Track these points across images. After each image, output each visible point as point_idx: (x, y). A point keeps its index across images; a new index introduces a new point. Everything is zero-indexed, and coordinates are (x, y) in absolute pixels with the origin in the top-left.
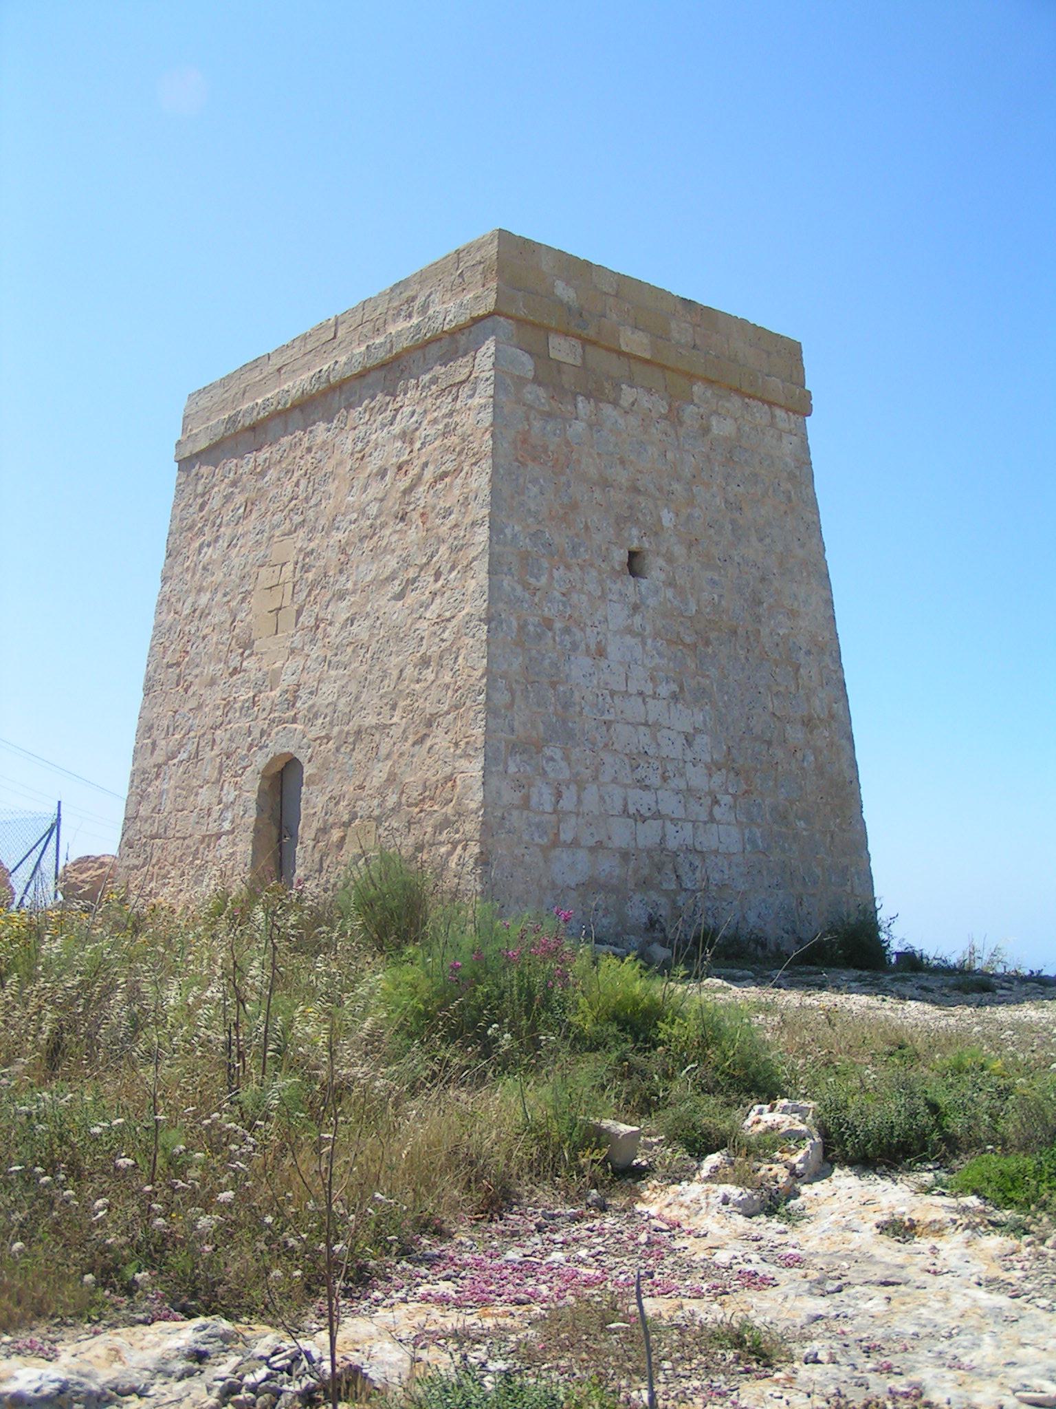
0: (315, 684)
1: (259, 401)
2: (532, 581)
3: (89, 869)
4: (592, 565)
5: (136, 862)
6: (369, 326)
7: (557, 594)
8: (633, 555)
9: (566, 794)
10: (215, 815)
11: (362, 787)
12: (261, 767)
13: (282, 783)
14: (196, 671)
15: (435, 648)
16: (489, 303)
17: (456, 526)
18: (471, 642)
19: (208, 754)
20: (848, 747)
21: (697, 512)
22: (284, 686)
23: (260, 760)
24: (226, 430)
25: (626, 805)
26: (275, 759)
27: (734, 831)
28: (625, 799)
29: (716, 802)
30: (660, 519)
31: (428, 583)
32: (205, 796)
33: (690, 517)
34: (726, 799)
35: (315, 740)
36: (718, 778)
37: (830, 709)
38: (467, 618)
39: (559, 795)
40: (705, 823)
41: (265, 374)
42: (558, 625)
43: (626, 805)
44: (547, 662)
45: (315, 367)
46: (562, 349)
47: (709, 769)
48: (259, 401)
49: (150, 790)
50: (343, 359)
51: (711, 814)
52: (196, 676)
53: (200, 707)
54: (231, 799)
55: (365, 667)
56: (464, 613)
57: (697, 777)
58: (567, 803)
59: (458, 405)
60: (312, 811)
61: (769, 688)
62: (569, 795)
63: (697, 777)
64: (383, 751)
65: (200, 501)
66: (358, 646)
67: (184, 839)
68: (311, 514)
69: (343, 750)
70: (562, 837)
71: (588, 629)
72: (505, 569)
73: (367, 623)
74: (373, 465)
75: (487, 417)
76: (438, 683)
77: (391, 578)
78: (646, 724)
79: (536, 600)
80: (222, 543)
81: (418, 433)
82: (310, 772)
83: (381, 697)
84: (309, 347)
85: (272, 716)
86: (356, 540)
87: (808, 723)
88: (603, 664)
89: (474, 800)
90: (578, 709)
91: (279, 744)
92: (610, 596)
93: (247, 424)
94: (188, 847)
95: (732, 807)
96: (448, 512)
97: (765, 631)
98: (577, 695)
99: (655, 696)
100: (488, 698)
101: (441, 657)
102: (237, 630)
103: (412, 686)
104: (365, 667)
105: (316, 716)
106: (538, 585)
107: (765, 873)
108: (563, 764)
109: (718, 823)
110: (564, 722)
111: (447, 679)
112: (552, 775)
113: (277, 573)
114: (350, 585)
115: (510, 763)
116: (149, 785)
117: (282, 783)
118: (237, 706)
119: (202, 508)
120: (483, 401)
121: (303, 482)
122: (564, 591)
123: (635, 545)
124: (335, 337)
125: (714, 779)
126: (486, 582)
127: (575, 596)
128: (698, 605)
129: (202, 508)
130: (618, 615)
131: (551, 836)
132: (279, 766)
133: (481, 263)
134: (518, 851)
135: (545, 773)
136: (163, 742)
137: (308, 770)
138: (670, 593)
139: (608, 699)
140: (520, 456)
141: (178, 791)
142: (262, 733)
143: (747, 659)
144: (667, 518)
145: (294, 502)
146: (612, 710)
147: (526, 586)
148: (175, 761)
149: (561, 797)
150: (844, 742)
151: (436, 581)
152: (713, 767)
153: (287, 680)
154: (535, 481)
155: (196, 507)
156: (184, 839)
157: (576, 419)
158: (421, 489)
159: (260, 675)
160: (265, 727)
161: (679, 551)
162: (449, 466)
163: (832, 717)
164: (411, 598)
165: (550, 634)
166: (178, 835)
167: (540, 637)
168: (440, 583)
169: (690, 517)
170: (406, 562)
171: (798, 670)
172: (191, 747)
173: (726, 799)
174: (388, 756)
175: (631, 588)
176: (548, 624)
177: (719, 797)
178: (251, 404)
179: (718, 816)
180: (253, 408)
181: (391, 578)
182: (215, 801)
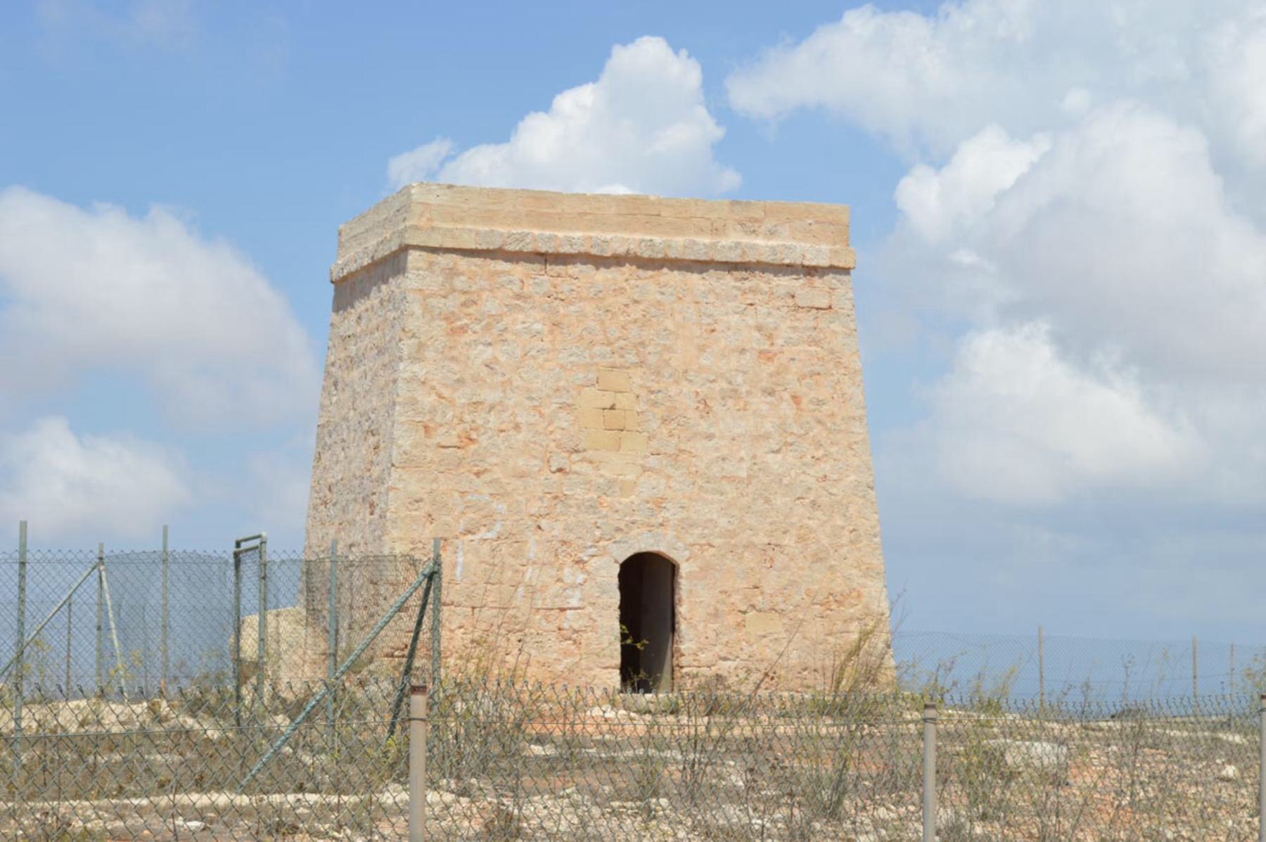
83: (771, 524)
137: (684, 569)
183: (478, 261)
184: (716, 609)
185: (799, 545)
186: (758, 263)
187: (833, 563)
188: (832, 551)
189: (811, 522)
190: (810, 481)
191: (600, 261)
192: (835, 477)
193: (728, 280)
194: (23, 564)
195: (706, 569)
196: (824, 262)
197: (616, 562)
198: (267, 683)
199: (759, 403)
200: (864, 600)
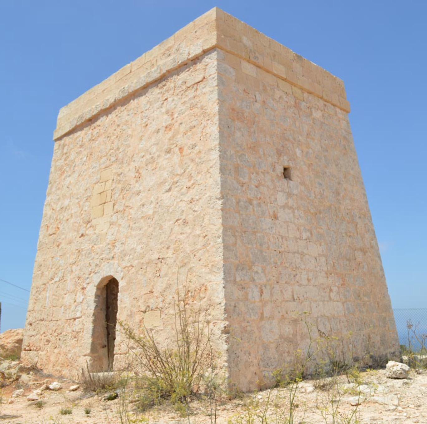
0: (124, 239)
1: (94, 107)
2: (241, 179)
3: (11, 336)
4: (268, 173)
5: (34, 333)
6: (149, 64)
7: (253, 186)
8: (285, 169)
9: (265, 291)
10: (73, 308)
11: (151, 292)
12: (96, 284)
13: (109, 290)
14: (63, 237)
15: (191, 216)
16: (213, 41)
17: (200, 152)
18: (211, 211)
19: (69, 277)
20: (379, 261)
21: (311, 151)
22: (108, 241)
23: (96, 279)
24: (77, 122)
25: (293, 296)
26: (103, 279)
27: (340, 304)
28: (293, 292)
29: (331, 290)
30: (295, 154)
31: (185, 182)
32: (68, 299)
33: (307, 153)
34: (335, 289)
35: (125, 268)
36: (330, 280)
37: (370, 243)
38: (209, 199)
39: (262, 292)
40: (328, 301)
41: (96, 94)
42: (255, 202)
43: (293, 296)
44: (251, 221)
45: (122, 87)
46: (248, 69)
47: (327, 274)
48: (94, 107)
49: (40, 297)
50: (135, 81)
51: (330, 297)
52: (63, 239)
53: (64, 254)
54: (81, 300)
55: (151, 229)
56: (207, 196)
57: (322, 279)
58: (266, 296)
59: (199, 92)
60: (124, 306)
61: (346, 233)
62: (266, 291)
63: (322, 279)
64: (162, 273)
65: (65, 156)
66: (146, 218)
67: (57, 321)
68: (120, 156)
69: (140, 272)
70: (265, 315)
71: (269, 204)
72: (228, 172)
73: (152, 206)
74: (153, 127)
75: (215, 96)
76: (193, 234)
77: (164, 182)
78: (298, 253)
79: (244, 189)
80: (76, 175)
81: (176, 110)
82: (122, 285)
83: (161, 243)
84: (118, 79)
85: (101, 257)
86: (144, 166)
87: (364, 251)
88: (277, 222)
89: (219, 296)
90: (267, 246)
91: (107, 271)
92: (277, 189)
93: (87, 118)
94: (59, 325)
95: (338, 293)
96: (194, 146)
97: (342, 207)
98: (266, 240)
99: (301, 238)
100: (224, 240)
101: (194, 221)
102: (83, 216)
103: (178, 237)
104: (151, 229)
105: (125, 255)
106: (244, 181)
107: (354, 324)
108: (262, 275)
109: (334, 301)
110: (261, 252)
111: (198, 232)
112: (257, 281)
113: (103, 186)
114: (141, 188)
115: (237, 275)
116: (40, 294)
117: (109, 290)
118: (83, 253)
119: (65, 160)
120: (211, 89)
121: (116, 141)
122: (256, 184)
123: (286, 164)
124: (131, 72)
125: (329, 279)
126: (219, 179)
127: (262, 188)
128: (315, 194)
129: (65, 160)
130: (281, 198)
131: (260, 314)
132: (106, 283)
133: (207, 24)
134: (243, 325)
135: (254, 280)
136: (47, 273)
137: (121, 284)
138: (303, 188)
139: (280, 240)
140: (231, 118)
141: (54, 297)
142: (97, 265)
143: (336, 220)
144: (298, 152)
145: (111, 151)
146: (283, 246)
147: (239, 182)
148: (53, 281)
149: (262, 292)
150: (377, 259)
151: (189, 181)
152: (328, 274)
153: (110, 238)
154: (239, 129)
155: (63, 159)
156: (57, 321)
157: (256, 102)
158: (178, 137)
159: (95, 236)
160: (98, 263)
161: (305, 168)
162: (194, 123)
163: (372, 247)
164: (175, 191)
165: (251, 207)
166: (54, 319)
167: (246, 208)
168: (192, 182)
169: (307, 153)
170: (173, 174)
171: (357, 225)
172: (60, 274)
173: (335, 289)
174: (166, 275)
175: (286, 185)
176: (250, 202)
177: (332, 288)
178: (89, 109)
179: (332, 297)
180: (90, 110)
181: (164, 182)
182: (72, 301)
183: (184, 57)
184: (131, 312)
185: (174, 255)
186: (168, 71)
187: (192, 265)
188: (192, 256)
189: (181, 237)
190: (183, 205)
191: (107, 111)
192: (197, 197)
193: (155, 92)
194: (288, 252)
195: (130, 282)
196: (199, 51)
197: (95, 286)
198: (329, 379)
199: (163, 161)
200: (208, 293)
